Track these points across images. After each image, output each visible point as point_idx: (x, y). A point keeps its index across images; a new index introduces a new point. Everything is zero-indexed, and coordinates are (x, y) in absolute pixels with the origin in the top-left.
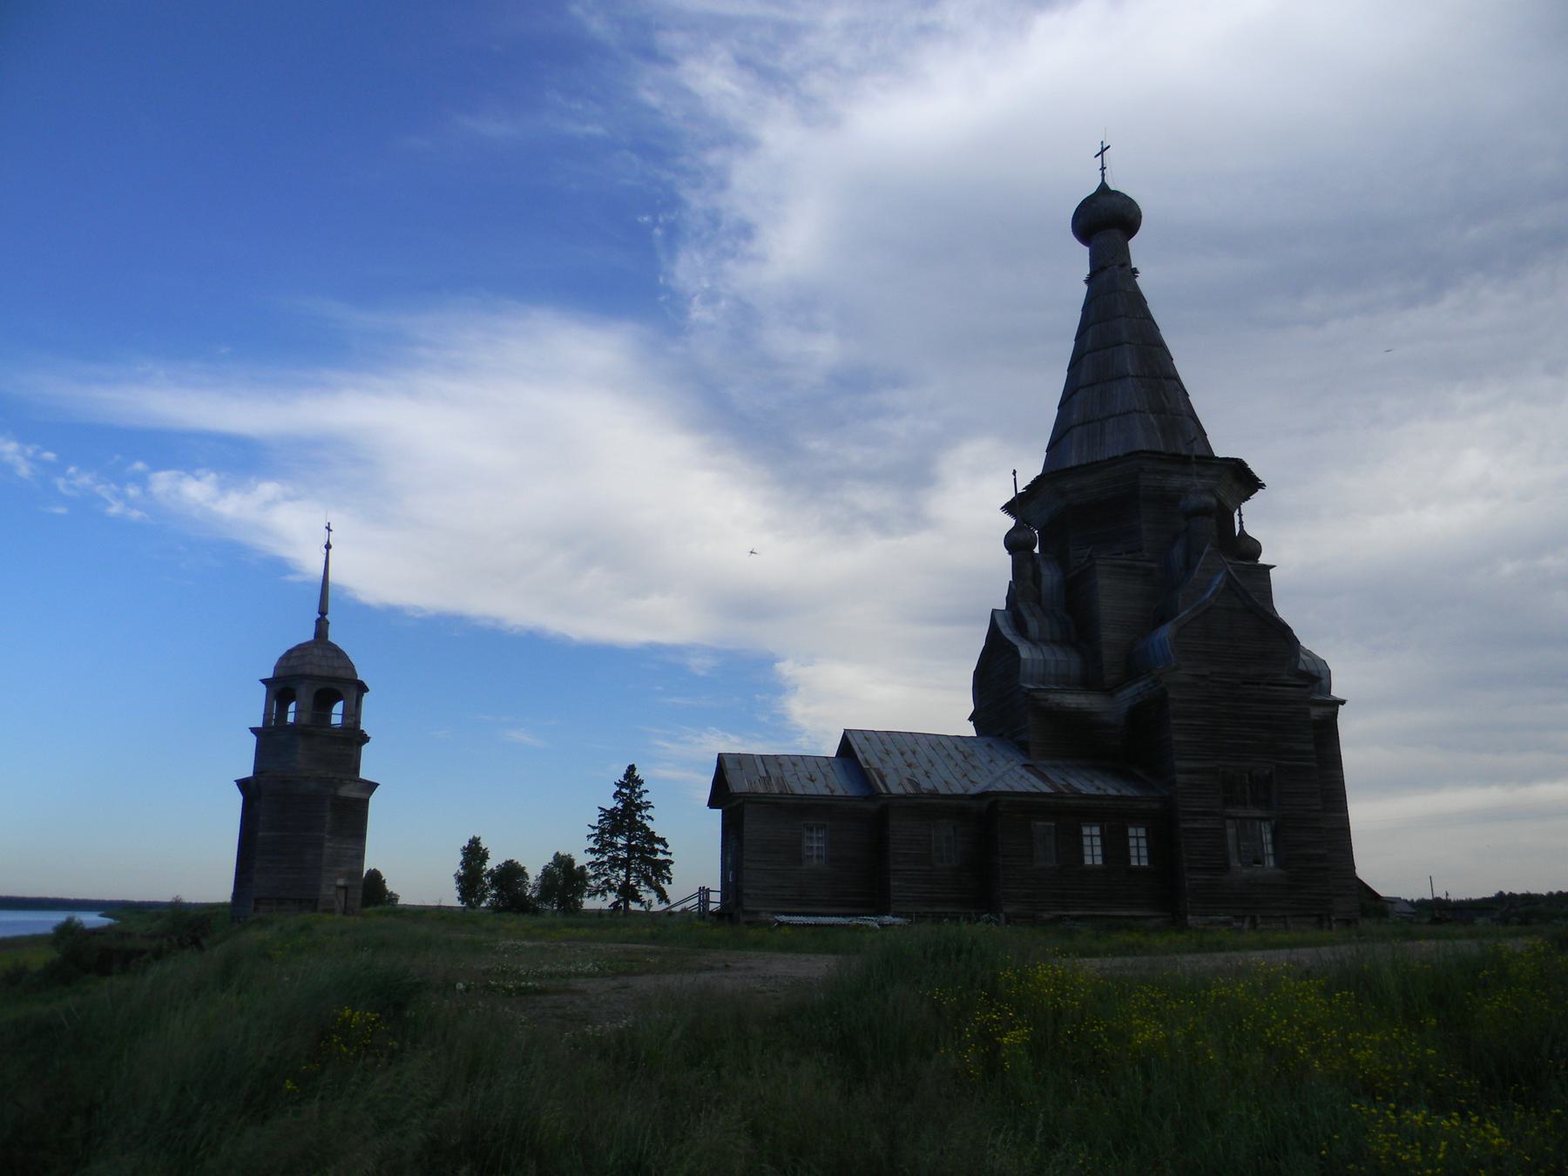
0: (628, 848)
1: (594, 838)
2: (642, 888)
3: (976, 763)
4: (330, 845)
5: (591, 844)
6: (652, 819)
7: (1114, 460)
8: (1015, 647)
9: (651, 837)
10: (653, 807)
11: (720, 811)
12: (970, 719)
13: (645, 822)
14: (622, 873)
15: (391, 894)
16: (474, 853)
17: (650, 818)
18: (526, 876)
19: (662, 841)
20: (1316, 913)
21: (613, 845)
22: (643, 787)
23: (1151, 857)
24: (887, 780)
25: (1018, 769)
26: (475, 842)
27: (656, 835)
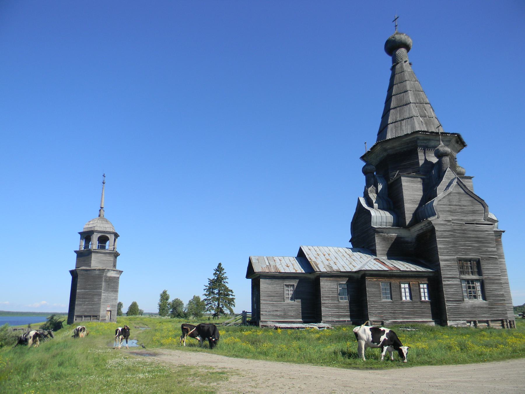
0: (219, 294)
1: (206, 290)
2: (224, 309)
3: (355, 259)
4: (104, 295)
5: (205, 292)
6: (228, 283)
7: (407, 135)
8: (369, 211)
9: (226, 289)
10: (228, 278)
11: (251, 279)
12: (350, 241)
13: (225, 284)
14: (216, 303)
15: (141, 310)
16: (164, 297)
17: (227, 282)
18: (183, 304)
19: (231, 291)
20: (501, 319)
21: (213, 293)
22: (224, 271)
23: (430, 297)
24: (319, 266)
25: (372, 260)
26: (165, 293)
27: (229, 289)
